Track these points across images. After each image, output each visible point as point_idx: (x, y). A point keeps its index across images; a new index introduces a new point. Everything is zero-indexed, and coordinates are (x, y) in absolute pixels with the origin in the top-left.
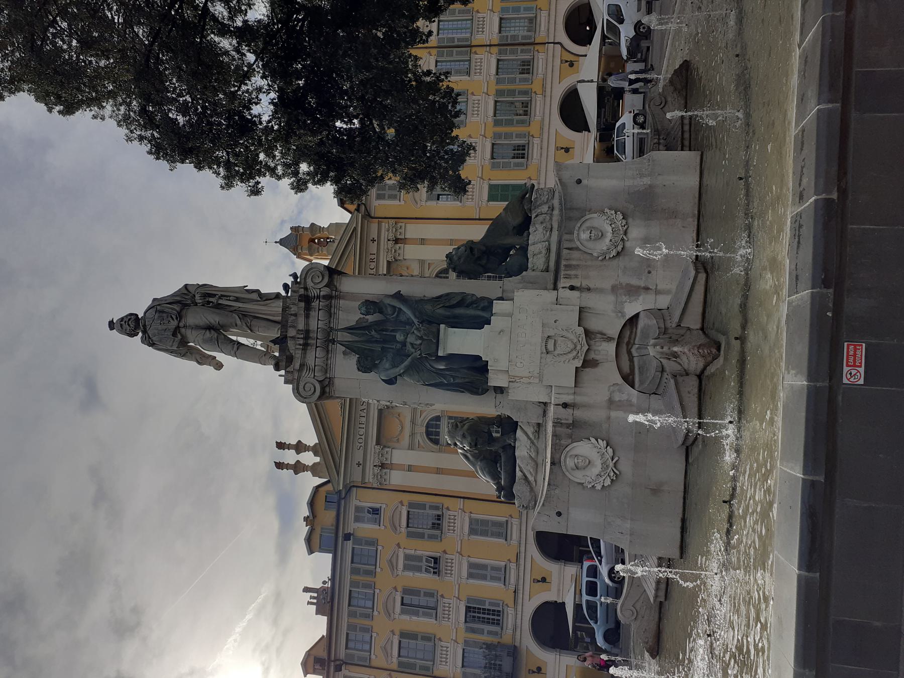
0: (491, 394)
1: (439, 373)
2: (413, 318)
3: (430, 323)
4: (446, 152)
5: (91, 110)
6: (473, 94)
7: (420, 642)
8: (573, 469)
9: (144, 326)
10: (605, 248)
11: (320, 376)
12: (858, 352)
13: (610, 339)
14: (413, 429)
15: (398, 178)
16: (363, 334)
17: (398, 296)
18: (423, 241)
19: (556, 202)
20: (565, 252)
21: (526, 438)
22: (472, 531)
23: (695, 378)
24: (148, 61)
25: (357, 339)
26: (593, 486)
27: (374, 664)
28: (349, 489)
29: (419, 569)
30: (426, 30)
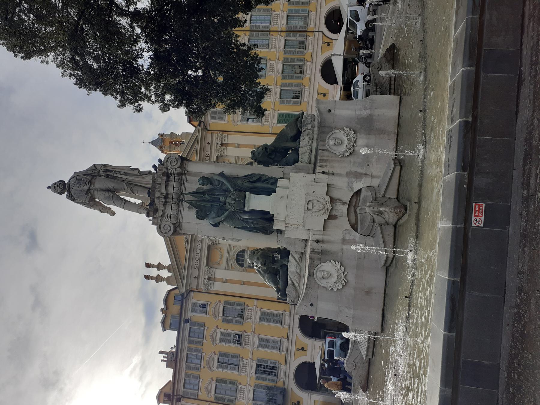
0: (275, 234)
1: (245, 221)
2: (230, 187)
3: (240, 191)
4: (253, 92)
5: (40, 58)
6: (270, 59)
7: (229, 386)
8: (321, 279)
9: (69, 188)
10: (343, 150)
11: (173, 221)
12: (481, 208)
13: (344, 203)
14: (228, 257)
15: (224, 106)
16: (200, 197)
17: (222, 174)
18: (238, 146)
19: (316, 123)
20: (320, 152)
21: (294, 261)
22: (261, 319)
23: (393, 227)
24: (76, 29)
25: (196, 199)
26: (332, 289)
27: (200, 397)
28: (189, 292)
29: (228, 341)
30: (243, 20)
